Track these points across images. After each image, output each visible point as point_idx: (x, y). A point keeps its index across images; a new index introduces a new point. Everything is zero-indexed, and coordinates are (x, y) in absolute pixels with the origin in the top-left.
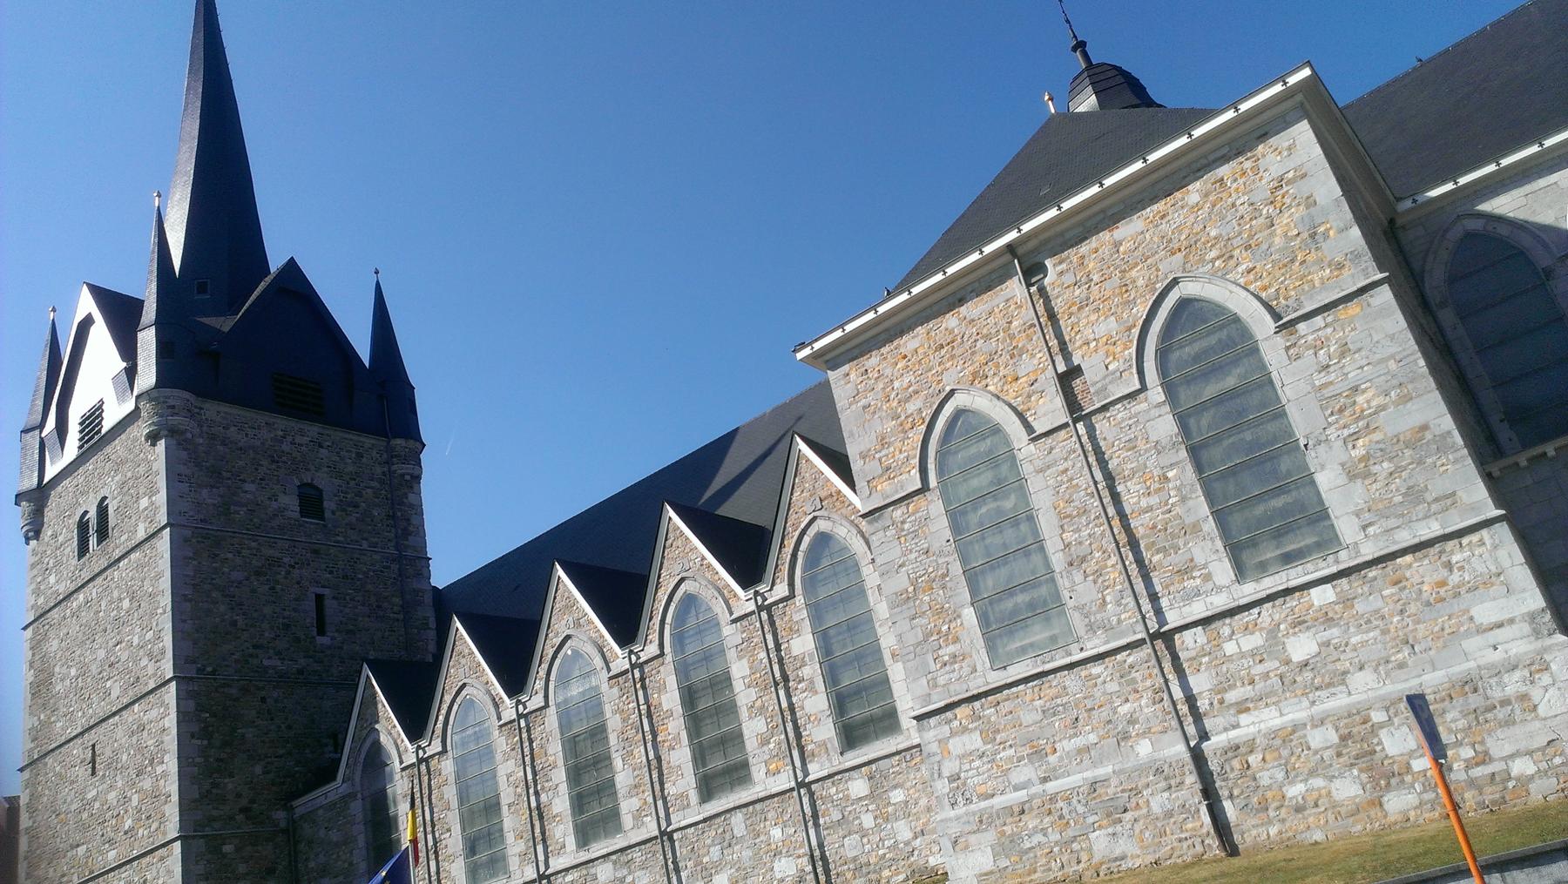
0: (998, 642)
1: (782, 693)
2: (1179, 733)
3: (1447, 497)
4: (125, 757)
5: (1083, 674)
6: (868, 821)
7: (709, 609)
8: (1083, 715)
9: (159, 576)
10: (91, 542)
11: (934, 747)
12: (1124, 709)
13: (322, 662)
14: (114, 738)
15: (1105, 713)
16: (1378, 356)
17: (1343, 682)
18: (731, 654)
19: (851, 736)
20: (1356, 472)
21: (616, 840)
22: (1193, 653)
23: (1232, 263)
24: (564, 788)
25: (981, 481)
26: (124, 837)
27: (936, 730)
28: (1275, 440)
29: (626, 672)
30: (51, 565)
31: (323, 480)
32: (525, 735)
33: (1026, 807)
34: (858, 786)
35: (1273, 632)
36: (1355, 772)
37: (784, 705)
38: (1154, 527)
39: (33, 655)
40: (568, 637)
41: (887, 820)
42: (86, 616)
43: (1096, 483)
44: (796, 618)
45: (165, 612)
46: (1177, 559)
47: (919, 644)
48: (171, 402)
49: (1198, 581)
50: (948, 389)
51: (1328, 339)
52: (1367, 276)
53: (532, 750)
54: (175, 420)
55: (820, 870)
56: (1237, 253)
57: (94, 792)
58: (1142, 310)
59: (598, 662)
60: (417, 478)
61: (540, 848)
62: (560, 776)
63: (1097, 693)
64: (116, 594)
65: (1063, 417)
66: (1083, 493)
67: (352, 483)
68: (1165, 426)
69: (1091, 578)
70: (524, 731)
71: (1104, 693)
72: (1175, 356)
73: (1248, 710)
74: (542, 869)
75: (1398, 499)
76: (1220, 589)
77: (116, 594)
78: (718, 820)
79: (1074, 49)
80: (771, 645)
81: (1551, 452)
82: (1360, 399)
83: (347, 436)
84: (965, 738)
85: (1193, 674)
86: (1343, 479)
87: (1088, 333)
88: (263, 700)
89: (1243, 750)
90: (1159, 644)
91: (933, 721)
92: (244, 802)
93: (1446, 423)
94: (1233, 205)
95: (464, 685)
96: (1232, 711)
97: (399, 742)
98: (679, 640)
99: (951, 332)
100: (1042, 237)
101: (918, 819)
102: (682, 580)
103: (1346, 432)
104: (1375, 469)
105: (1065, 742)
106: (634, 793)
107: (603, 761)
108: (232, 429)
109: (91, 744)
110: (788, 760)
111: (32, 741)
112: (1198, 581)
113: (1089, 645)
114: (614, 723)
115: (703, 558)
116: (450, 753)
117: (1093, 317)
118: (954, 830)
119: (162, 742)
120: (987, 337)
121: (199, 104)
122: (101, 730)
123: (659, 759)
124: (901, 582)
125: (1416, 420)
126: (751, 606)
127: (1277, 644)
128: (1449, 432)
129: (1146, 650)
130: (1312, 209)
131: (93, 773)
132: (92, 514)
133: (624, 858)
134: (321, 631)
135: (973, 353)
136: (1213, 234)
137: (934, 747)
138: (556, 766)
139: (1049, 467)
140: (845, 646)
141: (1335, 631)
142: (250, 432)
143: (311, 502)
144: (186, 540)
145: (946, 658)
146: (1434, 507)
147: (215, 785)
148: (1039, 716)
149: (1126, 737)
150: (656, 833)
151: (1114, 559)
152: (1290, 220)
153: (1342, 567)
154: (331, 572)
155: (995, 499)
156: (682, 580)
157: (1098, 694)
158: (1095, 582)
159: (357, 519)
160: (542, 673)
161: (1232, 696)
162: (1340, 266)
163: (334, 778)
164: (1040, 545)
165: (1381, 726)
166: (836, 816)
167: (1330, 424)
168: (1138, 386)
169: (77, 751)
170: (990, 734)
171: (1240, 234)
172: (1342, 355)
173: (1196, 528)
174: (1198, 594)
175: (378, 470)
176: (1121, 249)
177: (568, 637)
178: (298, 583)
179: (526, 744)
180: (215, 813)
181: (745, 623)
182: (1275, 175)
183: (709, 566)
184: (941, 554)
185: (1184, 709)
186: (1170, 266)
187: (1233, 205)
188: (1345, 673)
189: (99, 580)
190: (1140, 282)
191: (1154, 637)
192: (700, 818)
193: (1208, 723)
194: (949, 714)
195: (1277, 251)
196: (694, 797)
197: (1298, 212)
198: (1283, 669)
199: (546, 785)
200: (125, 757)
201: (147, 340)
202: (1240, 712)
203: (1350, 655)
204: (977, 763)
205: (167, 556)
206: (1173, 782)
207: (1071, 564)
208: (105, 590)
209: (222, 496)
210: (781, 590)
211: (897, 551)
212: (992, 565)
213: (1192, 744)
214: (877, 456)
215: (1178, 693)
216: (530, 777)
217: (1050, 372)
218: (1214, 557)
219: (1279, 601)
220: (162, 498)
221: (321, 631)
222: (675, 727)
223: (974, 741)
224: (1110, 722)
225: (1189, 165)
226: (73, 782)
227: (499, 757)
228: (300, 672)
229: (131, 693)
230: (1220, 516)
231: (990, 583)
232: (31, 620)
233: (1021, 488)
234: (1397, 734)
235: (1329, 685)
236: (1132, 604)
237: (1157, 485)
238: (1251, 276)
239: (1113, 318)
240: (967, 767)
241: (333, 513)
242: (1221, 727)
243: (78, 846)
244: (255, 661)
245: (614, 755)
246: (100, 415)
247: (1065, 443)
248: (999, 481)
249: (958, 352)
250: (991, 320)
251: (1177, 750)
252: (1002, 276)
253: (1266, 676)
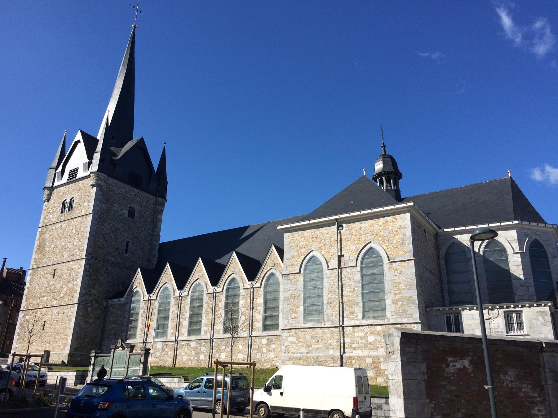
0: (306, 316)
1: (251, 311)
2: (339, 351)
3: (411, 314)
4: (65, 276)
5: (323, 330)
6: (264, 350)
7: (238, 283)
8: (320, 340)
9: (86, 227)
10: (66, 210)
11: (284, 338)
12: (330, 342)
13: (124, 261)
14: (63, 269)
15: (325, 341)
16: (407, 277)
17: (377, 349)
18: (241, 297)
19: (266, 328)
20: (394, 302)
21: (198, 337)
22: (348, 333)
23: (384, 242)
24: (187, 319)
25: (314, 276)
26: (60, 299)
27: (286, 334)
28: (380, 289)
29: (212, 293)
30: (51, 211)
31: (136, 207)
32: (180, 302)
33: (301, 358)
34: (264, 341)
35: (366, 333)
36: (373, 370)
37: (251, 315)
38: (349, 300)
39: (40, 237)
40: (198, 279)
41: (269, 351)
42: (60, 231)
43: (339, 285)
44: (260, 293)
45: (86, 238)
46: (352, 310)
47: (288, 311)
48: (100, 177)
49: (354, 316)
50: (312, 249)
51: (398, 269)
52: (411, 257)
53: (181, 306)
54: (100, 182)
55: (249, 359)
56: (385, 240)
57: (53, 283)
58: (362, 246)
59: (205, 288)
60: (162, 211)
61: (177, 333)
62: (187, 315)
63: (325, 336)
64: (71, 228)
65: (337, 267)
66: (335, 287)
67: (144, 209)
68: (358, 277)
69: (332, 308)
70: (180, 300)
71: (326, 336)
72: (365, 260)
73: (356, 350)
74: (177, 338)
75: (401, 311)
76: (358, 320)
77: (71, 228)
78: (226, 339)
79: (382, 147)
80: (252, 298)
81: (441, 309)
82: (400, 285)
83: (146, 194)
84: (292, 338)
85: (346, 338)
86: (391, 303)
87: (348, 248)
88: (107, 269)
89: (352, 359)
90: (341, 328)
91: (286, 331)
92: (96, 297)
93: (416, 297)
94: (388, 229)
95: (166, 283)
96: (352, 349)
97: (144, 292)
98: (228, 289)
99: (317, 235)
100: (344, 219)
101: (277, 353)
102: (233, 273)
103: (395, 292)
104: (398, 303)
105: (314, 345)
106: (206, 326)
107: (200, 314)
108: (115, 187)
109: (54, 269)
110: (248, 329)
112: (354, 316)
113: (326, 324)
114: (205, 306)
115: (240, 269)
116: (158, 300)
117: (350, 244)
118: (283, 359)
119: (77, 275)
120: (325, 240)
121: (123, 77)
122: (58, 266)
123: (215, 319)
124: (288, 295)
125: (410, 294)
126: (249, 286)
127: (366, 336)
128: (416, 300)
129: (338, 329)
130: (404, 236)
131: (53, 277)
132: (68, 201)
133: (199, 342)
134: (126, 252)
135: (321, 242)
136: (382, 234)
137: (284, 338)
138: (187, 313)
139: (330, 278)
140: (270, 304)
141: (379, 337)
142: (120, 189)
143: (131, 213)
144: (96, 219)
145: (293, 317)
146: (408, 316)
147: (90, 291)
148: (310, 337)
149: (328, 348)
150: (210, 338)
151: (338, 305)
152: (399, 237)
153: (385, 323)
154: (133, 235)
155: (316, 281)
156: (233, 273)
157: (325, 336)
158: (332, 309)
159: (143, 220)
160: (189, 286)
161: (353, 345)
162: (406, 252)
163: (123, 297)
164: (322, 297)
165: (382, 362)
166: (257, 347)
167: (392, 289)
168: (355, 265)
169: (50, 269)
170: (298, 338)
171: (388, 236)
172: (400, 274)
173: (358, 304)
174: (353, 319)
175: (152, 206)
176: (361, 229)
177: (198, 279)
178: (123, 237)
179: (180, 304)
180: (88, 299)
181: (247, 290)
182: (399, 225)
183: (241, 272)
184: (299, 291)
185: (342, 345)
186: (371, 238)
187: (388, 229)
188: (378, 347)
189: (67, 222)
190: (363, 239)
191: (341, 326)
192: (222, 337)
193: (346, 350)
194: (290, 331)
195: (394, 244)
196: (222, 331)
197: (401, 236)
198: (366, 343)
199: (183, 317)
200: (65, 276)
201: (97, 156)
202: (354, 350)
203: (380, 344)
205: (90, 222)
206: (335, 361)
207: (328, 303)
208: (68, 225)
209: (108, 207)
210: (258, 285)
211: (289, 286)
212: (311, 297)
213: (341, 354)
214: (291, 260)
215: (342, 341)
216: (179, 313)
217: (337, 254)
218: (359, 312)
219: (370, 326)
220: (92, 204)
221: (126, 252)
222: (221, 312)
223: (294, 339)
224: (325, 343)
225: (382, 214)
226: (46, 278)
227: (171, 305)
228: (118, 263)
229: (70, 258)
230: (363, 302)
231: (309, 301)
233: (322, 280)
234: (384, 364)
235: (374, 349)
236: (338, 317)
237: (352, 291)
238: (387, 247)
239: (354, 246)
240: (290, 345)
241: (137, 217)
242: (349, 352)
243: (44, 297)
244: (107, 257)
245: (203, 314)
246: (77, 172)
247: (335, 273)
248: (318, 277)
249: (317, 240)
250: (327, 236)
251: (338, 354)
252: (333, 224)
253: (362, 343)
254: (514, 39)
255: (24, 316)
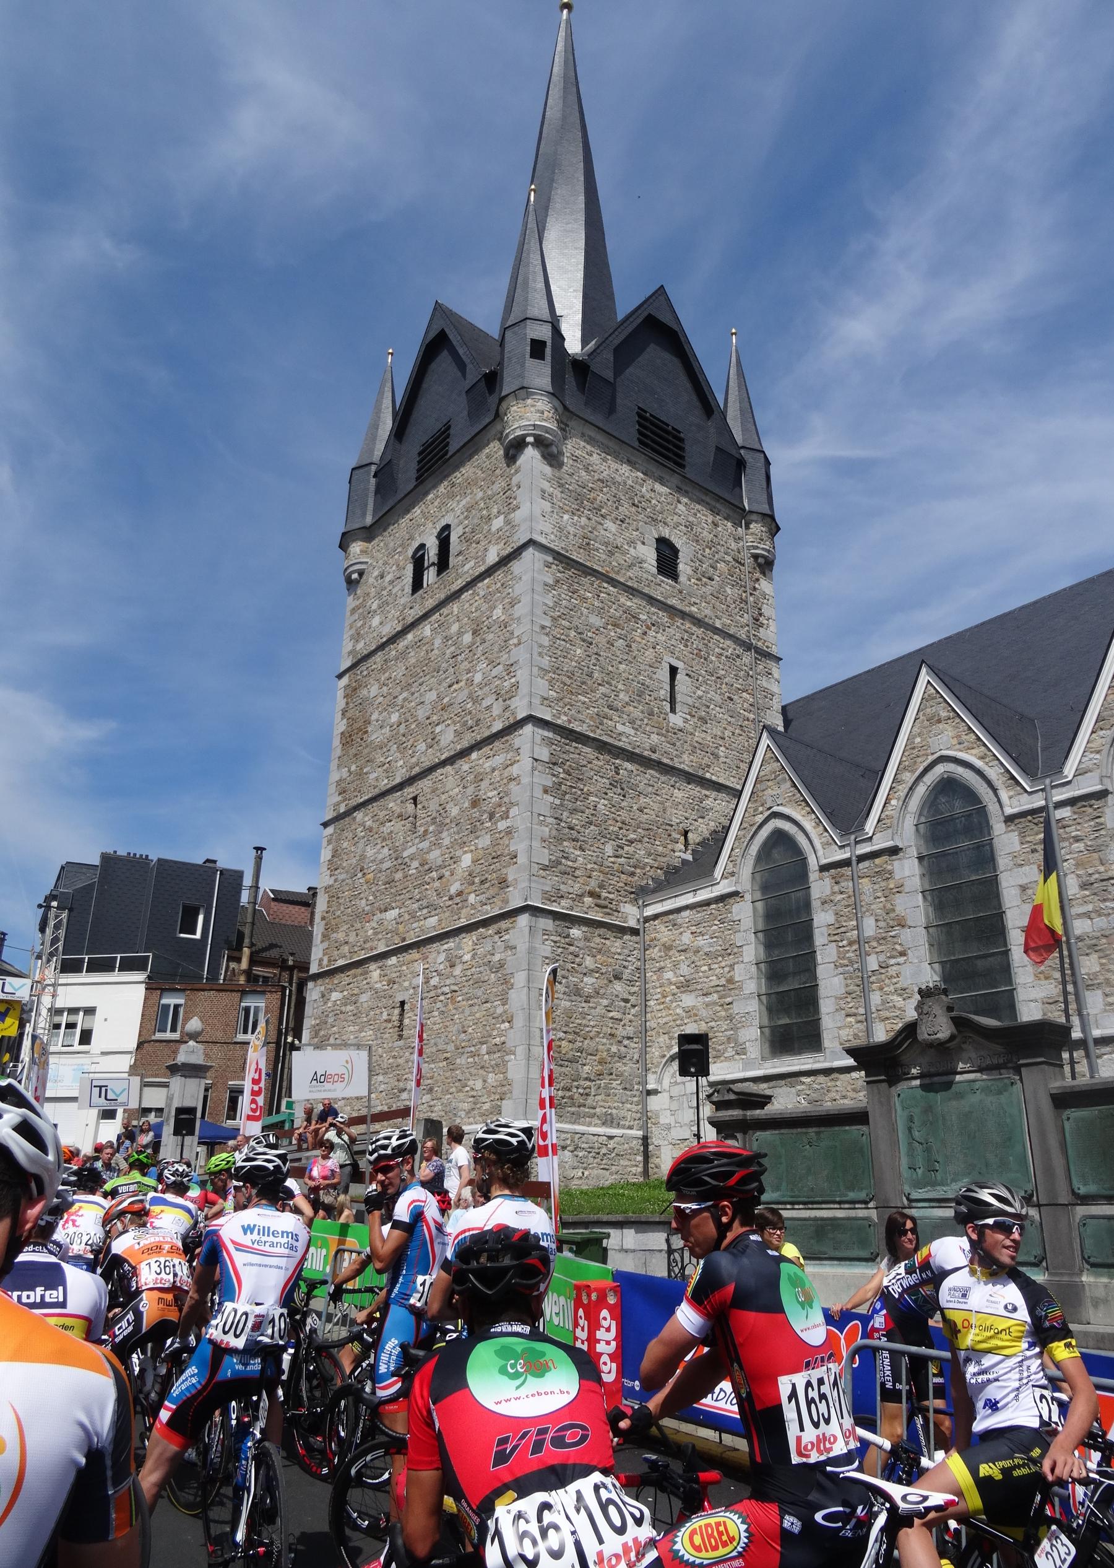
39: (347, 703)
64: (455, 628)
77: (455, 628)
111: (340, 794)
178: (654, 648)
204: (457, 1084)
232: (557, 305)
254: (173, 1250)
255: (323, 996)
